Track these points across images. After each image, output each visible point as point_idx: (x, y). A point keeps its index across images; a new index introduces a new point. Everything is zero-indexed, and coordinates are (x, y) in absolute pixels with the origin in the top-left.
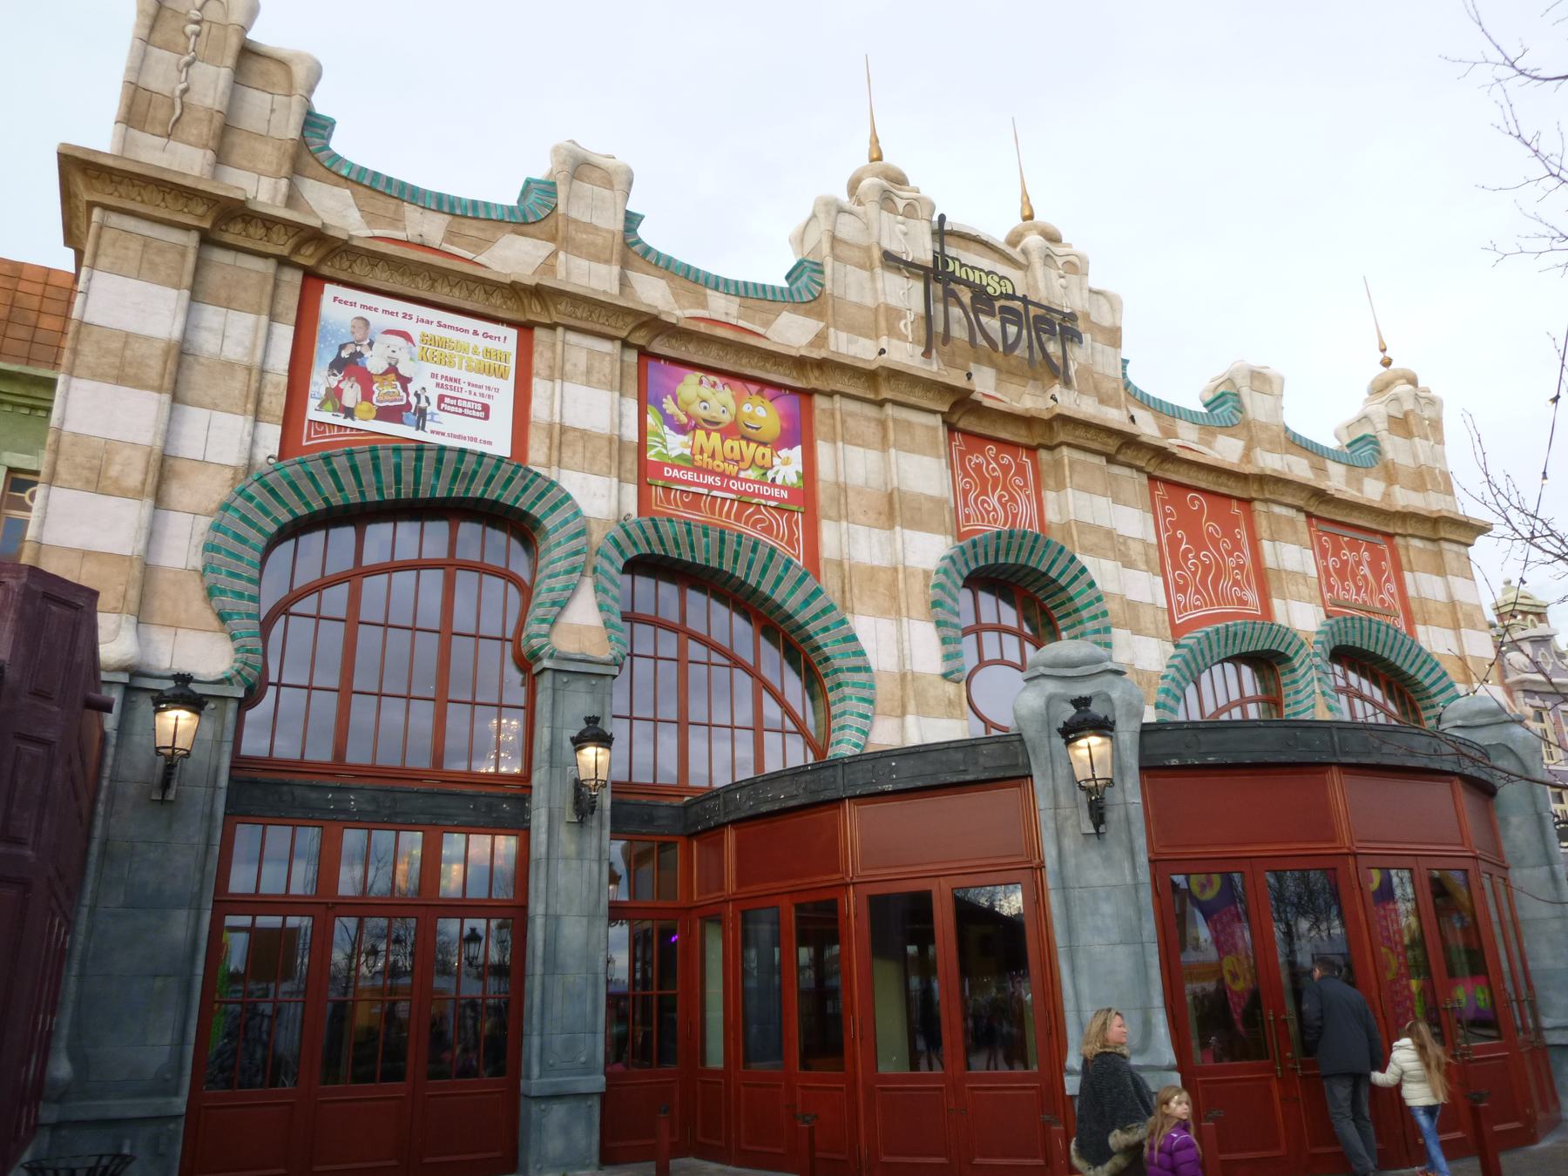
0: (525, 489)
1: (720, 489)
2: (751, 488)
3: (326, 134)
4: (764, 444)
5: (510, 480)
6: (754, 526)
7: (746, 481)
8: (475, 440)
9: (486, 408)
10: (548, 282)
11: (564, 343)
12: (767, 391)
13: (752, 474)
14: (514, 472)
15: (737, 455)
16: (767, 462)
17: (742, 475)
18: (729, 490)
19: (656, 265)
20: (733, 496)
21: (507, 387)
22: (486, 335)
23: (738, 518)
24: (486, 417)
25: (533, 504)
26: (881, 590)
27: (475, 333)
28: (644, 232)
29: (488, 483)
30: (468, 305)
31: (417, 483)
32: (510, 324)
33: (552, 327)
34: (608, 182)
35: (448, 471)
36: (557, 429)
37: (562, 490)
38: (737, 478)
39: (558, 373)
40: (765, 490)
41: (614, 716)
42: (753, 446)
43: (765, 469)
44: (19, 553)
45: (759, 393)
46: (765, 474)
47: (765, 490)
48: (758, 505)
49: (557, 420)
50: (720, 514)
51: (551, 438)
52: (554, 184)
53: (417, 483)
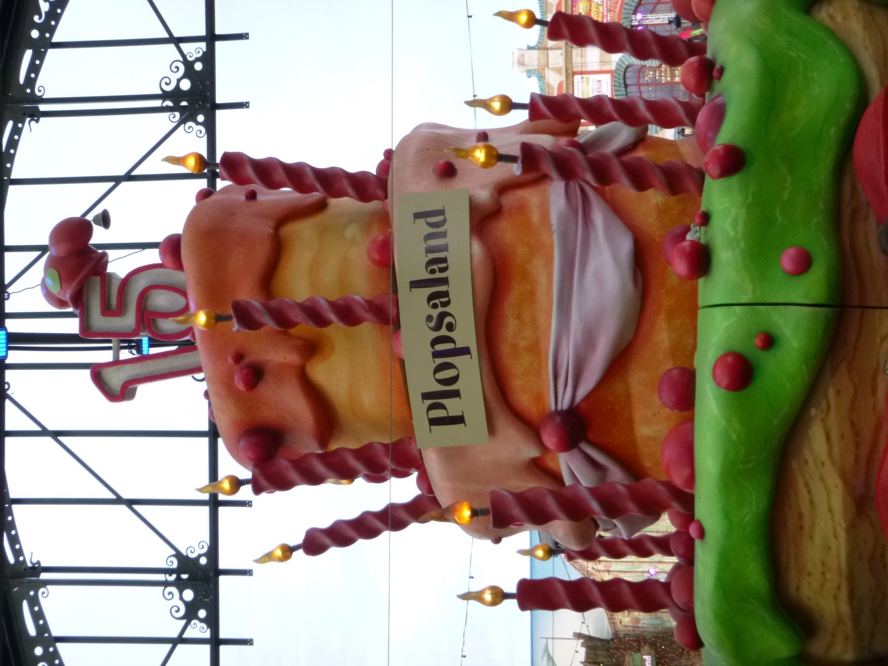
0: (620, 70)
1: (607, 17)
2: (605, 7)
3: (613, 88)
4: (591, 5)
5: (618, 74)
6: (616, 7)
7: (603, 10)
8: (607, 83)
9: (599, 81)
10: (564, 70)
11: (576, 64)
12: (574, 4)
13: (601, 8)
14: (616, 73)
15: (596, 13)
16: (596, 4)
17: (602, 11)
18: (607, 15)
19: (543, 39)
20: (609, 14)
21: (591, 77)
22: (578, 83)
23: (614, 12)
24: (601, 81)
25: (623, 67)
26: (669, 75)
27: (578, 86)
28: (533, 43)
29: (620, 79)
30: (572, 89)
31: (623, 95)
32: (573, 77)
33: (572, 67)
34: (523, 56)
35: (619, 88)
36: (601, 63)
37: (618, 61)
38: (603, 13)
39: (584, 64)
40: (605, 4)
41: (541, 638)
42: (592, 8)
43: (598, 5)
44: (662, 81)
45: (575, 7)
46: (600, 4)
47: (605, 4)
48: (610, 6)
49: (598, 64)
50: (614, 15)
51: (603, 65)
52: (527, 71)
53: (623, 95)
